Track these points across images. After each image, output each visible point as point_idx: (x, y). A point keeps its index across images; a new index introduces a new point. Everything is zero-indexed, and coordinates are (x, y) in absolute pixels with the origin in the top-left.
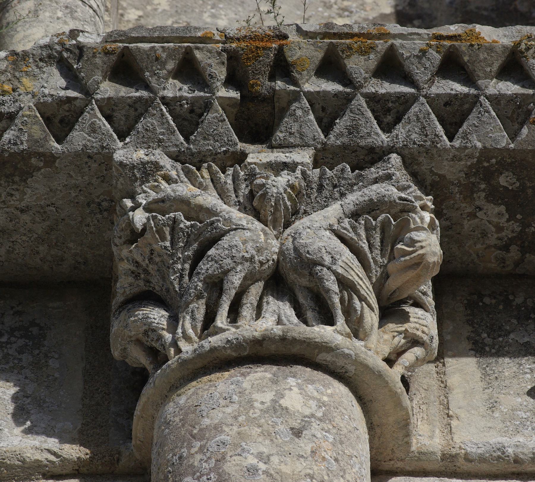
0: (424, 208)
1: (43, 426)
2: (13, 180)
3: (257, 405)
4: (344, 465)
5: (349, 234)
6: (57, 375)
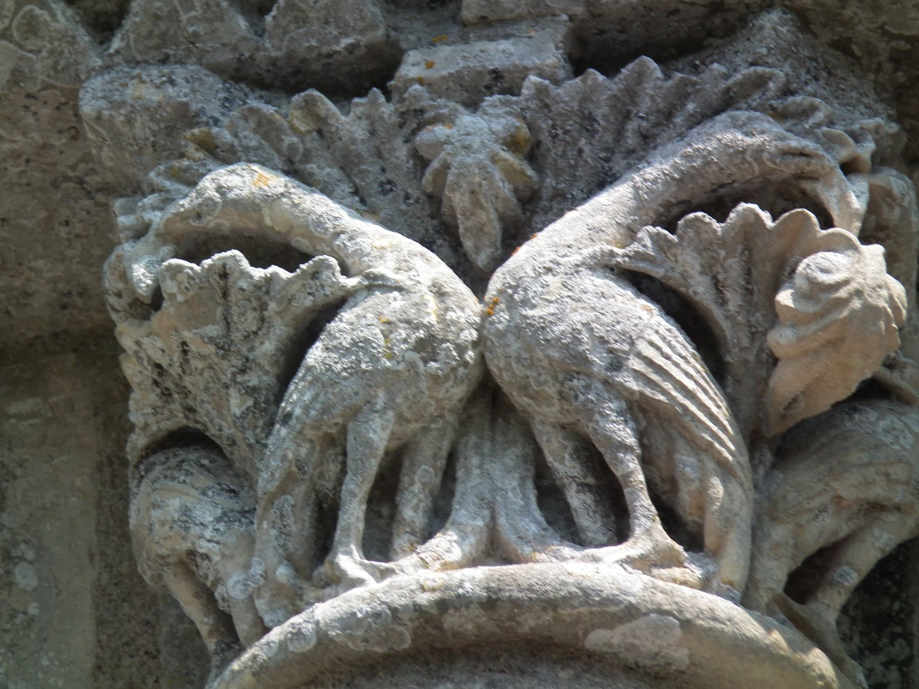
6: (33, 610)
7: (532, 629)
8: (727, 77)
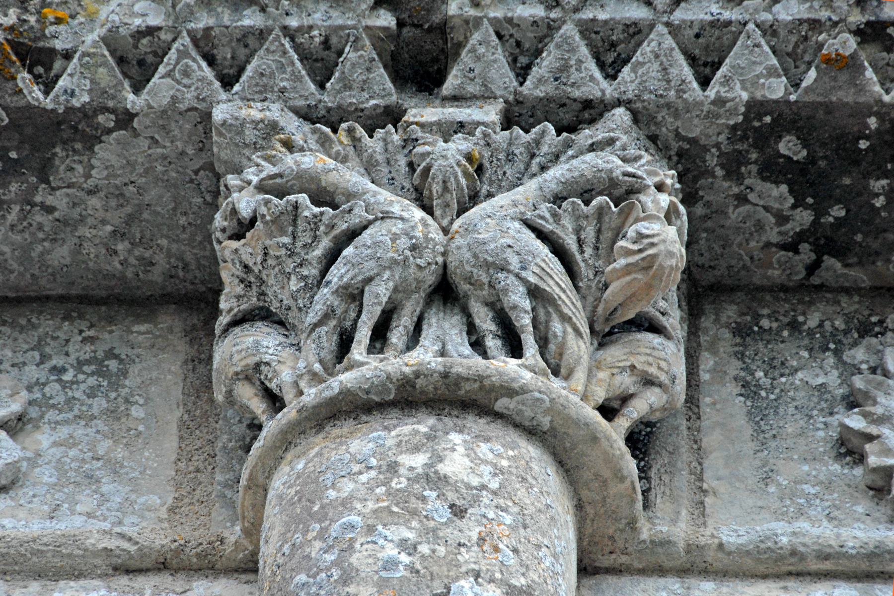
0: (660, 187)
1: (119, 500)
2: (72, 147)
3: (402, 471)
4: (527, 558)
5: (548, 226)
6: (141, 428)
7: (467, 392)
8: (591, 137)
